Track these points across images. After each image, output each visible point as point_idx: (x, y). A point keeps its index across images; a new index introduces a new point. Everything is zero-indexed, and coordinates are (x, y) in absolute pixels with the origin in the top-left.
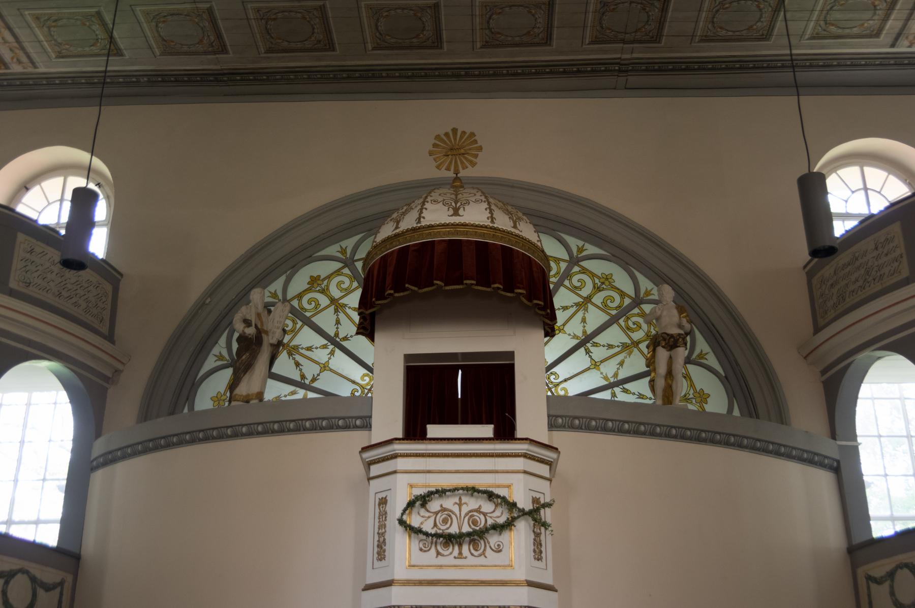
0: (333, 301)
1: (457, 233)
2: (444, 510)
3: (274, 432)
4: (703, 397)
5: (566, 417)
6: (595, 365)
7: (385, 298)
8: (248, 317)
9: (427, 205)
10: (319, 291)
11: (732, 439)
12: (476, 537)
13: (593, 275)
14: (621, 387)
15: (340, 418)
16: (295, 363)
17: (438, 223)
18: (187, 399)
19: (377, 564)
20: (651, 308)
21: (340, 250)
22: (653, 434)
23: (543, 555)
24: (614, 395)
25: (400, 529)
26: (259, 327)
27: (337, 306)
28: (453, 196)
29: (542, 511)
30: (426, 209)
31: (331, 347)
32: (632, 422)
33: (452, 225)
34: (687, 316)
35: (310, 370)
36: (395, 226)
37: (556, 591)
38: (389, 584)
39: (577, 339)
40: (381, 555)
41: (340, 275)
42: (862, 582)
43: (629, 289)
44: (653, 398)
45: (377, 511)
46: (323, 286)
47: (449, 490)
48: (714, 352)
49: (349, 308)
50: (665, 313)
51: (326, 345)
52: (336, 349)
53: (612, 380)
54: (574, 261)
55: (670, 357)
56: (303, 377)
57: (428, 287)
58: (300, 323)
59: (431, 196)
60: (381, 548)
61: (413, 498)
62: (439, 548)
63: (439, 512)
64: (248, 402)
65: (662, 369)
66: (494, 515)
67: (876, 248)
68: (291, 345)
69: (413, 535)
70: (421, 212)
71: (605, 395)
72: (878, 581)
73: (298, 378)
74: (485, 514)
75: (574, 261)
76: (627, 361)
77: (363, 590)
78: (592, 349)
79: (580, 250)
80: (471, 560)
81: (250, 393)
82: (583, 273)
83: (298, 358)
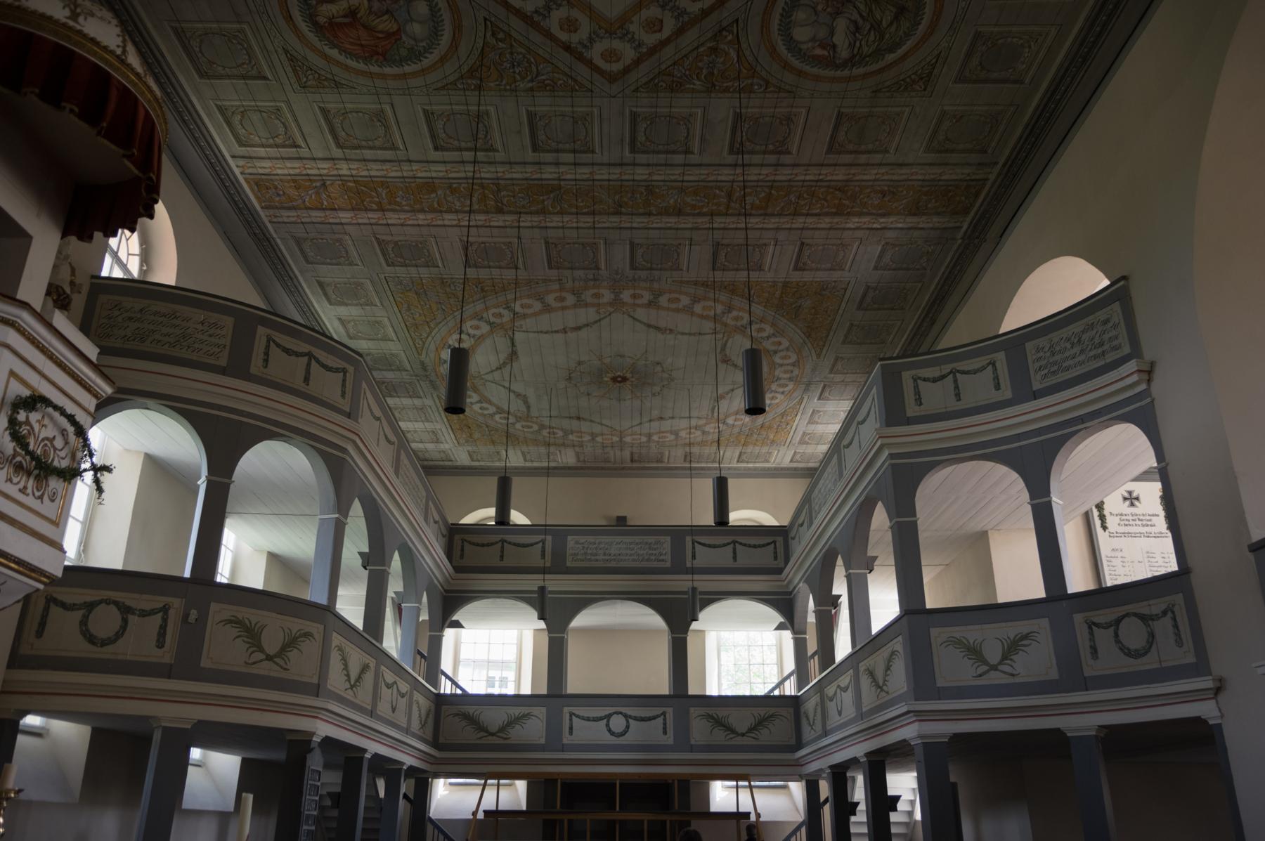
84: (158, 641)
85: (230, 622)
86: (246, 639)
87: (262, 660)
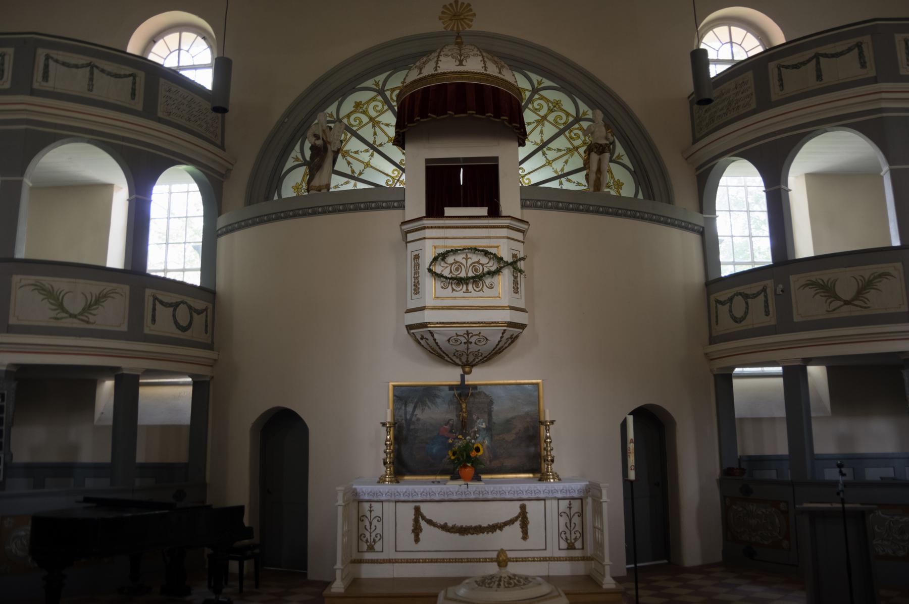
0: (371, 119)
1: (462, 78)
2: (456, 262)
3: (340, 211)
4: (619, 185)
5: (532, 200)
6: (549, 163)
7: (414, 123)
8: (317, 133)
9: (441, 58)
10: (361, 112)
11: (638, 214)
12: (477, 279)
13: (547, 101)
14: (566, 178)
15: (383, 202)
16: (347, 163)
17: (449, 71)
18: (277, 188)
19: (414, 296)
20: (588, 125)
21: (374, 83)
22: (587, 211)
23: (519, 290)
24: (561, 183)
25: (428, 274)
26: (325, 139)
27: (374, 122)
28: (458, 51)
29: (518, 263)
30: (440, 61)
31: (371, 151)
32: (575, 204)
33: (459, 72)
34: (612, 131)
35: (358, 167)
36: (418, 73)
37: (527, 312)
38: (422, 309)
39: (537, 145)
40: (416, 290)
41: (376, 101)
42: (713, 304)
43: (572, 111)
44: (587, 185)
45: (413, 263)
46: (364, 109)
47: (460, 250)
48: (628, 155)
49: (383, 124)
50: (597, 129)
51: (368, 149)
52: (375, 152)
53: (560, 173)
54: (535, 91)
55: (600, 159)
56: (353, 172)
57: (443, 115)
58: (349, 135)
59: (443, 51)
60: (416, 286)
61: (437, 255)
62: (454, 286)
63: (453, 263)
64: (320, 191)
65: (594, 167)
66: (488, 265)
67: (736, 88)
68: (344, 150)
69: (437, 278)
70: (437, 63)
71: (554, 185)
72: (722, 303)
73: (350, 173)
74: (482, 265)
75: (535, 91)
76: (570, 160)
77: (405, 313)
78: (547, 152)
79: (540, 83)
80: (474, 294)
81: (322, 184)
82: (542, 99)
83: (349, 159)
84: (765, 311)
85: (807, 285)
86: (822, 294)
87: (841, 306)
